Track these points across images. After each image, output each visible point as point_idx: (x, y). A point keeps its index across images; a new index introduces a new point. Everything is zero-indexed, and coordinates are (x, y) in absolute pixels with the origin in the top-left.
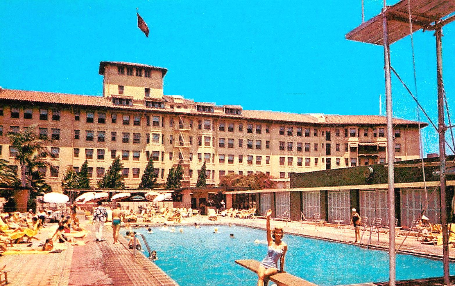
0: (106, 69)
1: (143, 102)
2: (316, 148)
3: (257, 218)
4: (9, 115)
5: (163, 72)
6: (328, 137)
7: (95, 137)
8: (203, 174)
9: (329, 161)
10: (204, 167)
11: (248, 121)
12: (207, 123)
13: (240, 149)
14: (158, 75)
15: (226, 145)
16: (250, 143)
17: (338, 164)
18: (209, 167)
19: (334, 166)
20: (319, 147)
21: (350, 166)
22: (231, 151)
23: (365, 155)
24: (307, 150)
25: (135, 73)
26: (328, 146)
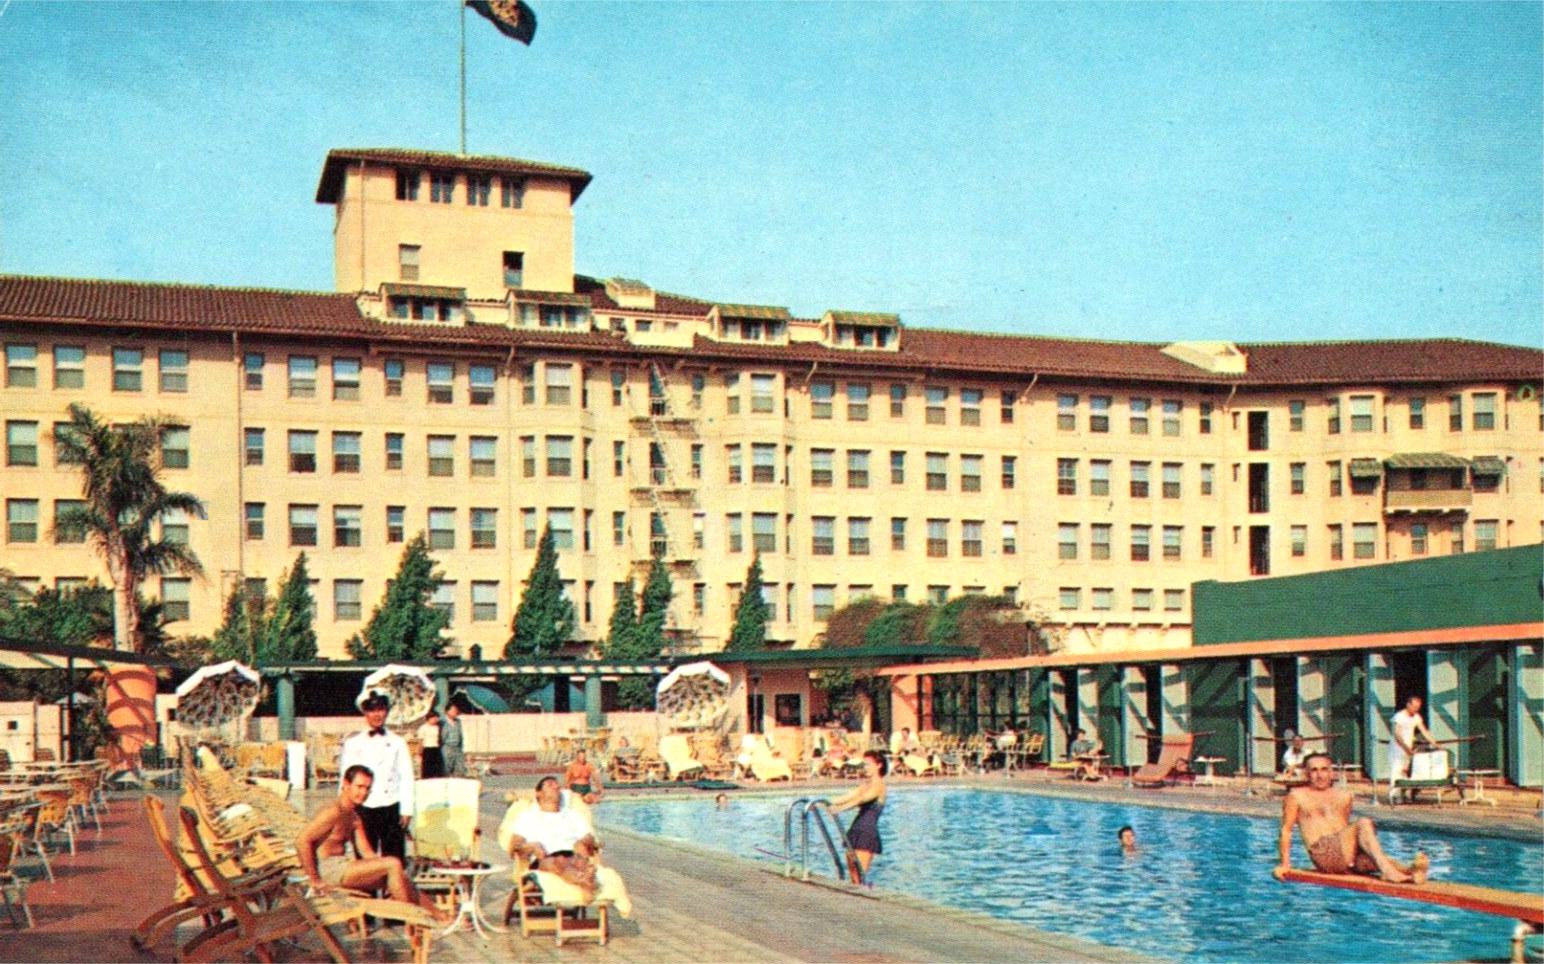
0: (353, 183)
1: (505, 303)
2: (1011, 476)
3: (515, 771)
4: (922, 415)
5: (576, 183)
6: (1257, 434)
7: (324, 456)
8: (752, 603)
9: (1259, 535)
10: (755, 571)
11: (928, 375)
12: (1483, 405)
13: (391, 478)
14: (558, 198)
15: (954, 482)
16: (936, 466)
17: (1298, 552)
18: (773, 568)
19: (1281, 564)
20: (1221, 476)
21: (1349, 561)
22: (858, 502)
23: (1414, 509)
24: (1171, 490)
25: (496, 192)
26: (1258, 473)
